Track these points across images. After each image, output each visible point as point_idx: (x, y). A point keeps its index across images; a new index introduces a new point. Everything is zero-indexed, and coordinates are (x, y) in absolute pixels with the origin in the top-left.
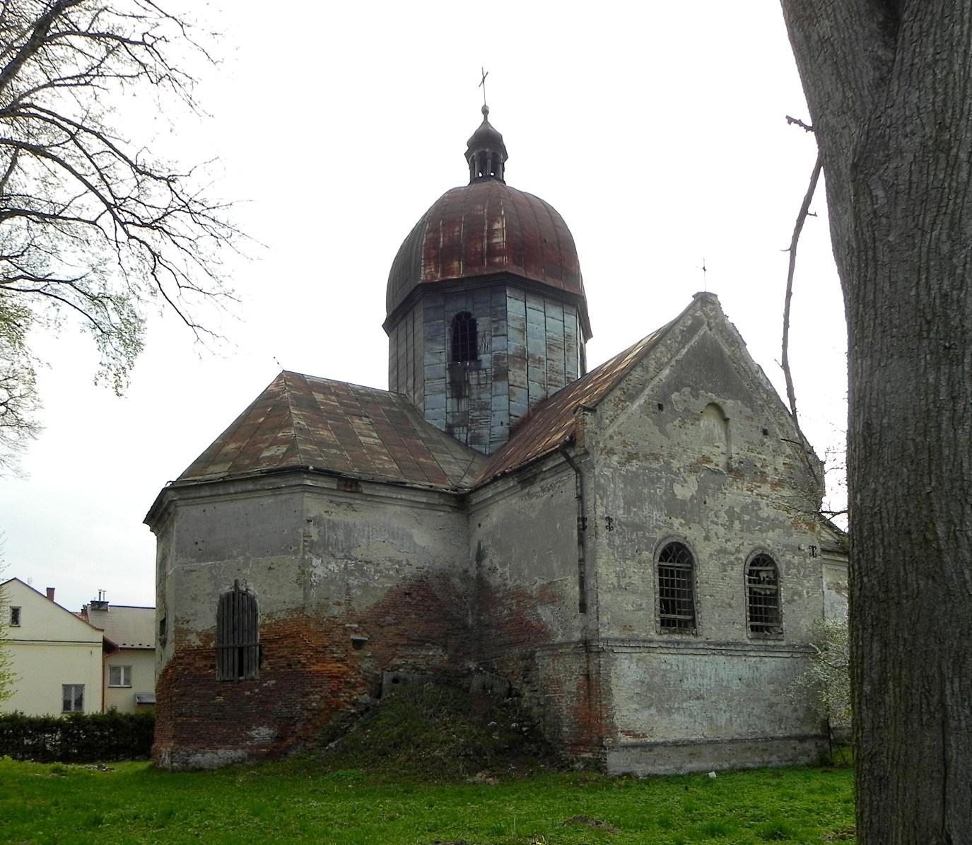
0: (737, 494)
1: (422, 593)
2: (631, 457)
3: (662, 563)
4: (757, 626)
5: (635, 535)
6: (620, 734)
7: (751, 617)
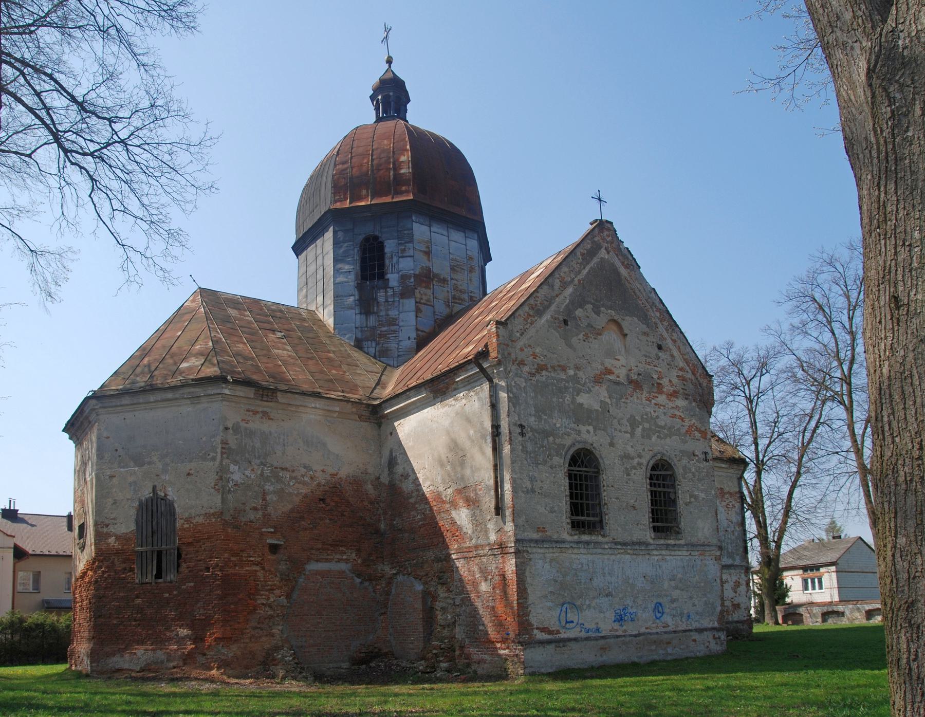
0: (637, 404)
1: (336, 499)
2: (541, 368)
3: (572, 468)
4: (658, 527)
5: (546, 442)
6: (536, 631)
7: (653, 519)
